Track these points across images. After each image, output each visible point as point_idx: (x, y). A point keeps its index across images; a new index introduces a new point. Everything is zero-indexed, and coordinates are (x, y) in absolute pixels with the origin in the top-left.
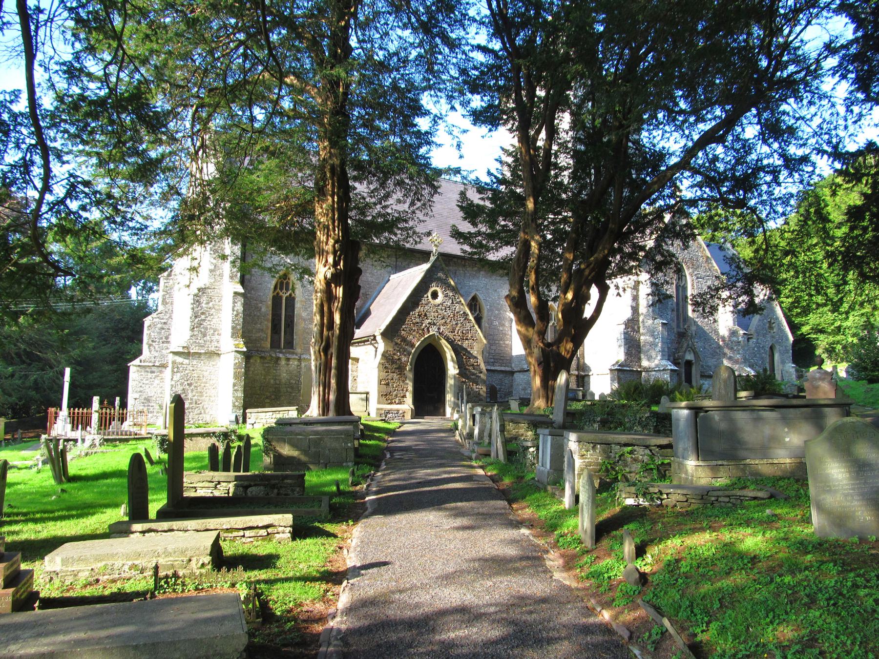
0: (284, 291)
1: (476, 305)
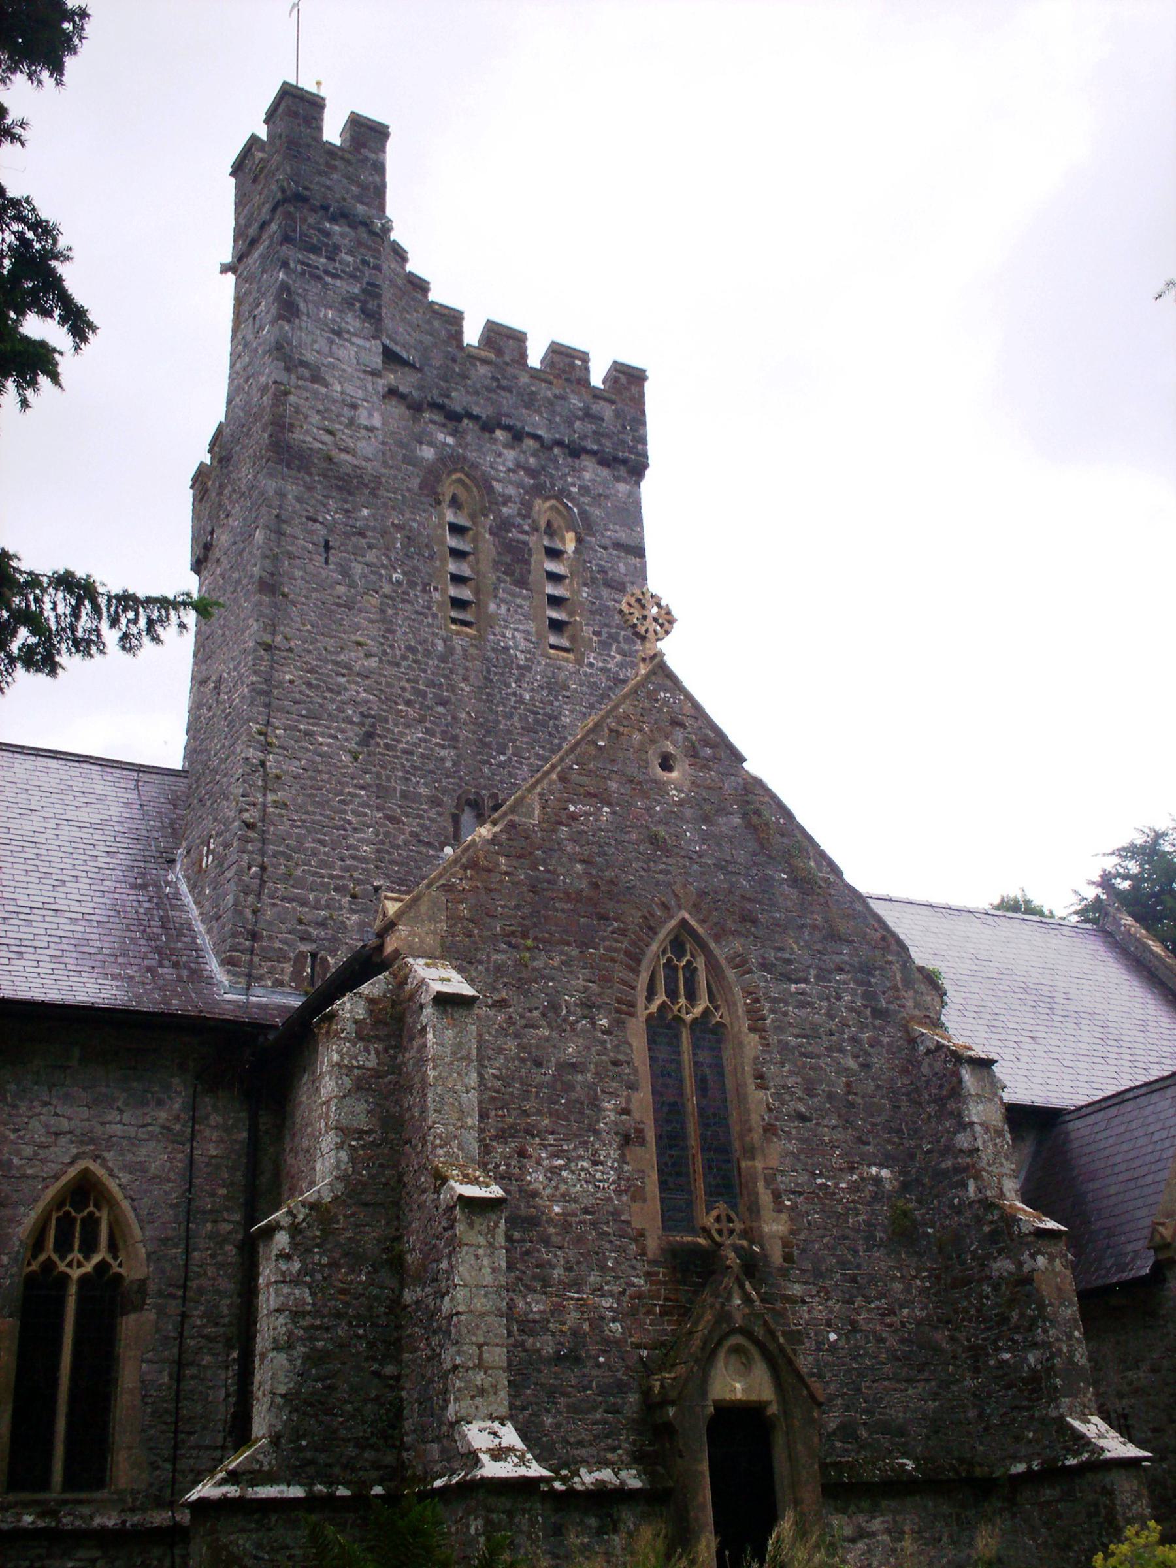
0: (76, 1255)
1: (91, 1224)
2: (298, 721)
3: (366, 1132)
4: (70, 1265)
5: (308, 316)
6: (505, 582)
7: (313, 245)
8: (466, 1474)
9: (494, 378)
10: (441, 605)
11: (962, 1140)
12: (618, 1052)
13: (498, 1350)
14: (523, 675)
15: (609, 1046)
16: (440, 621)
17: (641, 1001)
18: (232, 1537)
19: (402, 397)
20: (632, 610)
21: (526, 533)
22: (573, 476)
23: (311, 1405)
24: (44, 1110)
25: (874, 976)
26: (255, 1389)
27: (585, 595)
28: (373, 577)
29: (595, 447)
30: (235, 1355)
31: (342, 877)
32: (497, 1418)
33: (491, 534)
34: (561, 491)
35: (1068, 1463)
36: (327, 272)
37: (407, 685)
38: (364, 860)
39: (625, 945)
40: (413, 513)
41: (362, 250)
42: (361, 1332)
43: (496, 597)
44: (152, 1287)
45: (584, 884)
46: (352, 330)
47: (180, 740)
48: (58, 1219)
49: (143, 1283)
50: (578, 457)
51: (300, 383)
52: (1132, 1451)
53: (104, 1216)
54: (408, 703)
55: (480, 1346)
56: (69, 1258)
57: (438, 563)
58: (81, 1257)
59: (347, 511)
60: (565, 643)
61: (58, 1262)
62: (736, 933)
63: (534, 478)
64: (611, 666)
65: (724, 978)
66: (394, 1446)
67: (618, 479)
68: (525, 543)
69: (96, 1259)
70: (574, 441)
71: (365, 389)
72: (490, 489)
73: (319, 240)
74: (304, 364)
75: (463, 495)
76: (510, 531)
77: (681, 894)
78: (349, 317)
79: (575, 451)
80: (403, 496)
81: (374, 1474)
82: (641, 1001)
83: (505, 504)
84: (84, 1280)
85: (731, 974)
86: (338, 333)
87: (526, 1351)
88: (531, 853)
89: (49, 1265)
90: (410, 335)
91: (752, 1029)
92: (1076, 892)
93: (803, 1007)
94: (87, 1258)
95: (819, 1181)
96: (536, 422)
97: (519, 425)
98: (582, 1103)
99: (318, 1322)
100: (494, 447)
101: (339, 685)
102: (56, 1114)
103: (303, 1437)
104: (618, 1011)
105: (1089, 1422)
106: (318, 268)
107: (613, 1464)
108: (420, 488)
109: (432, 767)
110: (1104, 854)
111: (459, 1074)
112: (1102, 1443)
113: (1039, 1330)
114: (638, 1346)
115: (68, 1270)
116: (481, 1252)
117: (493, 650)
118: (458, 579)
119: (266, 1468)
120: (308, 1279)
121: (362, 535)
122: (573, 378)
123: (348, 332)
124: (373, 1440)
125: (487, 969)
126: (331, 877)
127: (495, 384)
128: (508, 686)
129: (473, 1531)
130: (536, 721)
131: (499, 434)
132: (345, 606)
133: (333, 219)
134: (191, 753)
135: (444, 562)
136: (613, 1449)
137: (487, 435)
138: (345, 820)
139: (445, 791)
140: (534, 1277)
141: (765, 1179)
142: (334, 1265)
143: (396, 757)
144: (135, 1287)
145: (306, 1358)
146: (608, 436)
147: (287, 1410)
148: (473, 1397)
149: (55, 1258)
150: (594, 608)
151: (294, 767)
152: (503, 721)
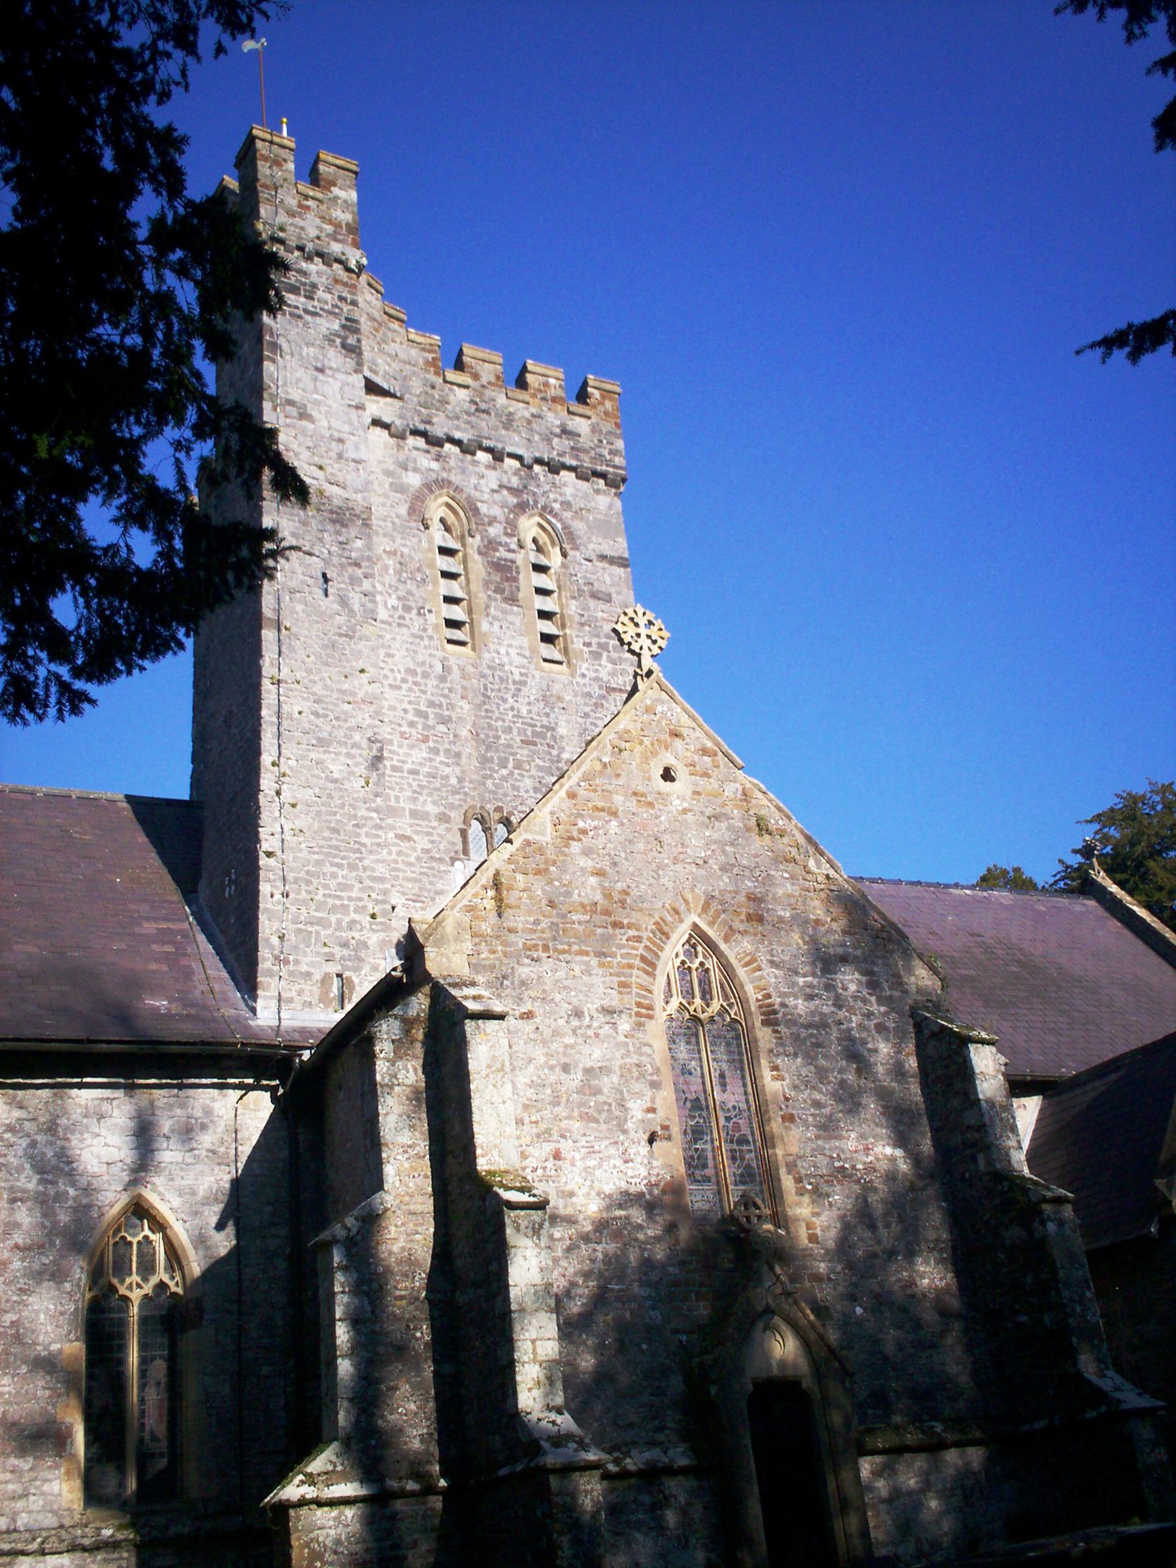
0: (135, 1278)
2: (309, 750)
3: (410, 1146)
5: (292, 355)
6: (495, 600)
7: (291, 285)
8: (529, 1462)
9: (473, 402)
10: (436, 627)
12: (641, 1054)
14: (519, 690)
15: (632, 1049)
16: (436, 642)
17: (659, 1002)
19: (386, 426)
20: (625, 629)
21: (513, 551)
22: (555, 492)
24: (95, 1142)
25: (877, 965)
26: (323, 1395)
27: (573, 608)
28: (370, 606)
29: (574, 463)
30: (291, 1363)
31: (361, 899)
33: (480, 553)
34: (544, 508)
35: (1087, 1416)
36: (306, 311)
37: (409, 707)
38: (382, 880)
39: (641, 951)
40: (402, 538)
41: (339, 287)
43: (488, 615)
45: (598, 897)
46: (334, 366)
47: (186, 768)
50: (558, 473)
51: (288, 421)
52: (1146, 1402)
54: (412, 724)
55: (533, 1342)
56: (128, 1280)
57: (430, 587)
58: (139, 1279)
59: (341, 543)
60: (557, 656)
61: (118, 1286)
62: (743, 933)
63: (516, 496)
64: (603, 675)
65: (736, 976)
67: (598, 492)
68: (513, 562)
69: (154, 1280)
70: (553, 459)
71: (350, 423)
72: (476, 511)
73: (297, 280)
74: (290, 403)
75: (451, 519)
76: (497, 550)
77: (689, 897)
78: (331, 352)
79: (554, 468)
80: (393, 523)
82: (659, 1002)
83: (490, 524)
85: (742, 973)
86: (321, 370)
88: (546, 870)
90: (389, 365)
91: (765, 1023)
92: (1060, 861)
93: (812, 999)
94: (146, 1279)
95: (837, 1164)
96: (514, 443)
97: (500, 446)
98: (610, 1105)
100: (477, 469)
101: (345, 713)
102: (106, 1145)
104: (638, 1014)
105: (1105, 1376)
106: (297, 307)
107: (661, 1443)
108: (409, 514)
109: (438, 785)
110: (1087, 822)
111: (495, 1086)
112: (1118, 1395)
113: (1053, 1293)
114: (677, 1331)
115: (127, 1293)
117: (489, 667)
118: (450, 600)
121: (358, 565)
122: (549, 397)
123: (331, 368)
125: (512, 983)
126: (350, 899)
127: (474, 408)
128: (505, 701)
129: (539, 1514)
130: (535, 734)
131: (482, 456)
132: (346, 636)
133: (309, 259)
134: (196, 782)
135: (436, 583)
136: (661, 1429)
137: (469, 457)
138: (359, 843)
139: (451, 807)
141: (787, 1165)
143: (402, 778)
146: (586, 451)
150: (583, 620)
151: (307, 795)
152: (503, 737)
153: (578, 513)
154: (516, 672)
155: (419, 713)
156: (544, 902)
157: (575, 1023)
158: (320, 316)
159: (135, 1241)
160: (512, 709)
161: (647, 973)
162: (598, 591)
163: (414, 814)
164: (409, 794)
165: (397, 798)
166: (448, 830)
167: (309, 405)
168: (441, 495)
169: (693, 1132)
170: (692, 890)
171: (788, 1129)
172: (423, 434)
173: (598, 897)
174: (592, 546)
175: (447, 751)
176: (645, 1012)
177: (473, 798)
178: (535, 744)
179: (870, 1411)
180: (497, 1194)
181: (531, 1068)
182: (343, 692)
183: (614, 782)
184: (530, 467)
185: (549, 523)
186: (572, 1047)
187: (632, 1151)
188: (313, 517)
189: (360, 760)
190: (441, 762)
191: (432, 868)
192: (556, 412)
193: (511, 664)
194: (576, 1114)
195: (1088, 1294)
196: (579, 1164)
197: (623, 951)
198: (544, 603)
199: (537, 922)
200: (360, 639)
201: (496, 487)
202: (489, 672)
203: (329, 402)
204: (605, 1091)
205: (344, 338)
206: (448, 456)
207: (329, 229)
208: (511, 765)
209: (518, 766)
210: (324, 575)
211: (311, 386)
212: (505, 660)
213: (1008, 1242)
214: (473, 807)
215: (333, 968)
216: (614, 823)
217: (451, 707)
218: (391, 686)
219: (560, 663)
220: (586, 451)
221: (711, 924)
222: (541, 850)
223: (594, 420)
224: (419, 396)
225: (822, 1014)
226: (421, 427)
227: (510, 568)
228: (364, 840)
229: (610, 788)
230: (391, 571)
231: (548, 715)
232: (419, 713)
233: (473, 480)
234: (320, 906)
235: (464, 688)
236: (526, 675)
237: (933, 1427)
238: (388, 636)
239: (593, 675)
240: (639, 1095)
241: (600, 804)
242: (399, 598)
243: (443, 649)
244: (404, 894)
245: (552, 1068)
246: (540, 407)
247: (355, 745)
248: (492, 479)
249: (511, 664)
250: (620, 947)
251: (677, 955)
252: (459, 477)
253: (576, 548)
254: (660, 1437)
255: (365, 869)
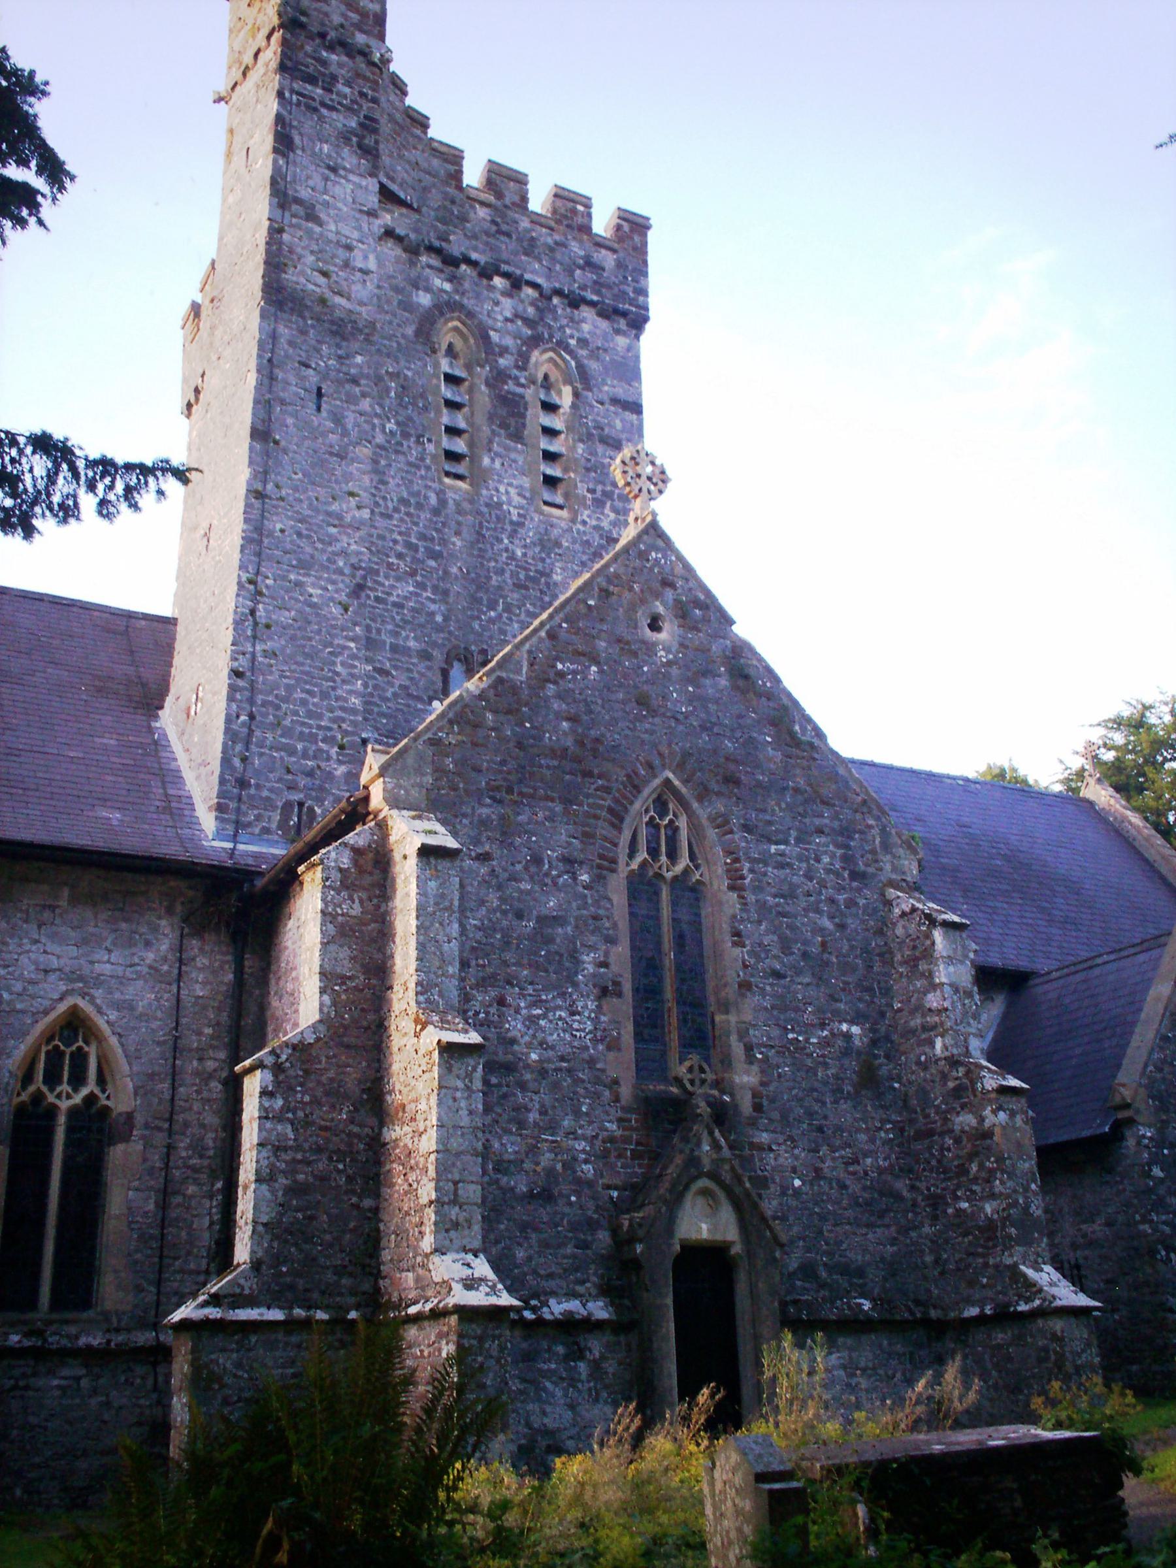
0: (65, 1087)
1: (80, 1059)
4: (59, 1096)
5: (303, 150)
9: (493, 222)
11: (933, 1000)
13: (472, 1187)
17: (622, 858)
18: (213, 1357)
19: (399, 239)
21: (523, 386)
23: (291, 1233)
29: (595, 298)
30: (219, 1185)
31: (330, 729)
32: (470, 1250)
33: (487, 384)
35: (1019, 1309)
36: (323, 104)
37: (399, 538)
38: (354, 711)
41: (360, 81)
42: (341, 1166)
43: (490, 450)
44: (139, 1119)
45: (569, 742)
47: (170, 586)
48: (48, 1053)
49: (130, 1116)
51: (294, 220)
52: (1083, 1300)
53: (92, 1051)
54: (400, 556)
55: (456, 1183)
56: (59, 1089)
60: (559, 500)
61: (48, 1093)
64: (605, 524)
66: (371, 1274)
67: (618, 332)
69: (85, 1092)
74: (298, 201)
75: (459, 344)
80: (399, 343)
81: (352, 1300)
83: (501, 355)
84: (73, 1112)
86: (334, 170)
87: (500, 1188)
88: (518, 710)
89: (38, 1098)
96: (535, 271)
97: (518, 272)
98: (561, 955)
99: (299, 1156)
101: (330, 536)
102: (45, 952)
103: (284, 1263)
104: (599, 867)
106: (313, 99)
111: (441, 924)
112: (1054, 1291)
114: (609, 1187)
115: (57, 1102)
116: (458, 1094)
117: (487, 505)
119: (247, 1292)
120: (290, 1115)
123: (344, 169)
124: (350, 1269)
126: (319, 727)
127: (494, 228)
128: (500, 541)
130: (528, 578)
131: (498, 281)
132: (337, 455)
135: (439, 413)
137: (485, 282)
139: (434, 644)
140: (509, 1121)
141: (739, 1032)
142: (316, 1102)
144: (122, 1120)
145: (288, 1190)
146: (609, 287)
147: (268, 1237)
148: (447, 1231)
149: (45, 1089)
153: (595, 354)
154: (514, 512)
155: (409, 545)
156: (512, 744)
157: (533, 869)
158: (337, 110)
159: (68, 1051)
160: (507, 550)
161: (613, 825)
162: (608, 436)
163: (394, 649)
164: (389, 627)
165: (379, 631)
166: (429, 668)
167: (318, 207)
168: (452, 319)
169: (646, 991)
170: (669, 745)
171: (743, 996)
172: (438, 251)
173: (569, 742)
174: (606, 388)
175: (435, 589)
176: (606, 866)
177: (456, 638)
178: (527, 588)
179: (799, 1283)
180: (1024, 1275)
181: (483, 911)
182: (329, 514)
183: (598, 626)
184: (550, 299)
185: (563, 359)
186: (529, 893)
187: (580, 1004)
188: (313, 326)
189: (341, 586)
190: (428, 598)
191: (408, 706)
192: (581, 242)
193: (509, 504)
194: (525, 961)
195: (1033, 1186)
196: (524, 1012)
197: (591, 801)
198: (551, 443)
199: (503, 762)
200: (353, 460)
201: (509, 315)
202: (485, 510)
203: (340, 205)
204: (558, 940)
205: (362, 138)
206: (462, 278)
207: (354, 17)
208: (500, 608)
209: (508, 608)
210: (319, 389)
211: (320, 185)
212: (504, 498)
213: (957, 1128)
214: (456, 647)
215: (296, 797)
216: (594, 668)
217: (444, 542)
218: (382, 514)
219: (560, 507)
220: (609, 287)
221: (685, 782)
222: (515, 689)
223: (621, 254)
224: (436, 210)
225: (791, 884)
226: (437, 243)
227: (517, 404)
228: (339, 668)
229: (594, 632)
230: (393, 394)
231: (543, 560)
232: (409, 545)
233: (487, 306)
234: (288, 732)
235: (459, 523)
236: (524, 516)
237: (861, 1305)
238: (383, 462)
239: (594, 523)
240: (592, 948)
241: (580, 648)
242: (398, 423)
243: (441, 482)
244: (377, 729)
245: (504, 913)
246: (565, 235)
247: (340, 572)
248: (507, 306)
249: (509, 504)
250: (588, 796)
251: (647, 811)
252: (472, 302)
253: (589, 389)
254: (580, 1289)
255: (338, 699)
